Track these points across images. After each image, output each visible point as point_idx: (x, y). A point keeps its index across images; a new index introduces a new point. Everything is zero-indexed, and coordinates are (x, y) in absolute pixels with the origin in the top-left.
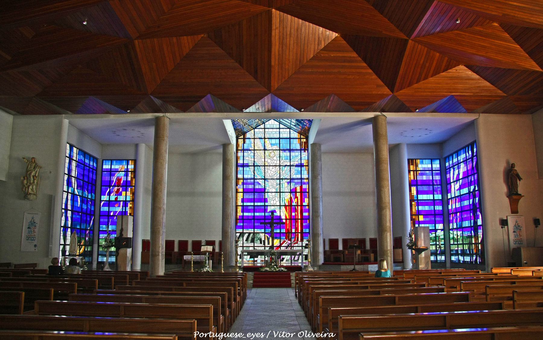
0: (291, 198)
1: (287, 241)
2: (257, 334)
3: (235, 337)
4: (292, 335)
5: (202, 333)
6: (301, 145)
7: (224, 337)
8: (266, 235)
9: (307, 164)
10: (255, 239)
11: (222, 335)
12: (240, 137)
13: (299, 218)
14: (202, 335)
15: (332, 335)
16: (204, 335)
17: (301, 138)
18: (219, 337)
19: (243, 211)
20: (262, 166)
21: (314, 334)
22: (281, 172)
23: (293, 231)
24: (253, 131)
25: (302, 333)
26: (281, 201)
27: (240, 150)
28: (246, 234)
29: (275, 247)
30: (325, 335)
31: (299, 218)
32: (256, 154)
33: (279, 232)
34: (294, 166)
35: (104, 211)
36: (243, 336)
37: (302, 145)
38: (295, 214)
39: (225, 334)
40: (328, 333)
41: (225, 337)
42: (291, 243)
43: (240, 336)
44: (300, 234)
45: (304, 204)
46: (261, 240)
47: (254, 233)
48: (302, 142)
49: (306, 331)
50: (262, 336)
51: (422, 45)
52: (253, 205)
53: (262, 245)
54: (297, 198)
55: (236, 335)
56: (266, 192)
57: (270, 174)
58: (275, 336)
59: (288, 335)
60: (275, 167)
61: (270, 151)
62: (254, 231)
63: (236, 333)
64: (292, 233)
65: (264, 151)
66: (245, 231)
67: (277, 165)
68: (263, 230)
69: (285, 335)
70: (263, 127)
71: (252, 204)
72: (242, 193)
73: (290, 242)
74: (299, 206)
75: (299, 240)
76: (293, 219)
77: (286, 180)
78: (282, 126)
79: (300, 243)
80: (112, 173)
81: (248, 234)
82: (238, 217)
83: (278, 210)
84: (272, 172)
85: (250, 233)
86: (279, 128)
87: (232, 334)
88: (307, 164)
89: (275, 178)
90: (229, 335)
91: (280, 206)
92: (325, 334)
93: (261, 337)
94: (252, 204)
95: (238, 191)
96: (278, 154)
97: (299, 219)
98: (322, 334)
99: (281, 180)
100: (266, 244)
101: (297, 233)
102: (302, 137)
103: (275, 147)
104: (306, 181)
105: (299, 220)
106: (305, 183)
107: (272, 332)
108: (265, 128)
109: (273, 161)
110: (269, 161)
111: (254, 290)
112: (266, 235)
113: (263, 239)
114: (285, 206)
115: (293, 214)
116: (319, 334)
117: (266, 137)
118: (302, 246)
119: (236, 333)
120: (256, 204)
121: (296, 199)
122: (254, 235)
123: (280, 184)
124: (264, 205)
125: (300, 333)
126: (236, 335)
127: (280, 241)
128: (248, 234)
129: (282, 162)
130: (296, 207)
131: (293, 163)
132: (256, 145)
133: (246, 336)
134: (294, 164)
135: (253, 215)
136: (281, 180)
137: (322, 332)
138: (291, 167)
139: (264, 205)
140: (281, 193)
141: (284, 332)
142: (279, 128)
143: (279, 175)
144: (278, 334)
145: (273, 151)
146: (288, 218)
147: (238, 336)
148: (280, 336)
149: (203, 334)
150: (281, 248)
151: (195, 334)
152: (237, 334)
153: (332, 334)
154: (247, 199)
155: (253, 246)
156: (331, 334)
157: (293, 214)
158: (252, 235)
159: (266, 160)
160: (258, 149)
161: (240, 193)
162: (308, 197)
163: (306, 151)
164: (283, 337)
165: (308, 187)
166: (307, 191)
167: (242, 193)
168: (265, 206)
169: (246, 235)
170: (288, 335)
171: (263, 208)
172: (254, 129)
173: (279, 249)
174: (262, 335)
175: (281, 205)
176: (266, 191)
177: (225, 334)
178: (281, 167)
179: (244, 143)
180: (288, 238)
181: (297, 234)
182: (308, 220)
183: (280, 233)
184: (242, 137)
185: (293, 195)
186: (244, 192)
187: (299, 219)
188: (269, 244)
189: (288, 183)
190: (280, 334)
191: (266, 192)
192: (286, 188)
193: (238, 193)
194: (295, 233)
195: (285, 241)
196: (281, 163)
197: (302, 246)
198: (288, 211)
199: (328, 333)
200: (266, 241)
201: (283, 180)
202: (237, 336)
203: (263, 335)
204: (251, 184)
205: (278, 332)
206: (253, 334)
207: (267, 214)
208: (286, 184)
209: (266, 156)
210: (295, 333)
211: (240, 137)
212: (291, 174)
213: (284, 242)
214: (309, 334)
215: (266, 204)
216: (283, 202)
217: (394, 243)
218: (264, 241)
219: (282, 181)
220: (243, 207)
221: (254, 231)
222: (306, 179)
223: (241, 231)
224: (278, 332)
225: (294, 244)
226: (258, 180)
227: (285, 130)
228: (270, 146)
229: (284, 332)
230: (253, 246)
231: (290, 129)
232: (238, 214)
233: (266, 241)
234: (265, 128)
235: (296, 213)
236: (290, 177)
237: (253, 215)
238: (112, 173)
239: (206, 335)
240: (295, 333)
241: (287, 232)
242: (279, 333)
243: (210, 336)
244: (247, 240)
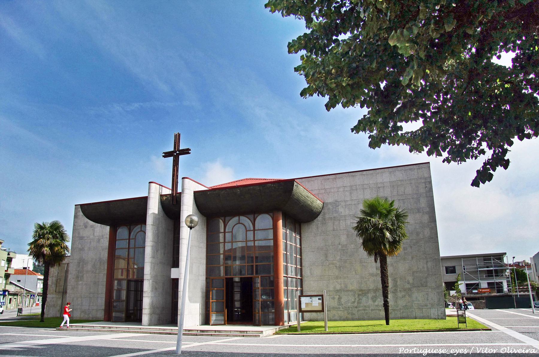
2: (461, 350)
3: (465, 353)
35: (143, 315)
40: (530, 349)
51: (114, 270)
55: (440, 351)
62: (254, 243)
80: (140, 283)
90: (433, 351)
92: (527, 350)
111: (504, 262)
125: (503, 349)
141: (487, 348)
152: (441, 350)
174: (440, 351)
206: (456, 350)
217: (277, 263)
221: (254, 243)
229: (487, 348)
238: (140, 283)
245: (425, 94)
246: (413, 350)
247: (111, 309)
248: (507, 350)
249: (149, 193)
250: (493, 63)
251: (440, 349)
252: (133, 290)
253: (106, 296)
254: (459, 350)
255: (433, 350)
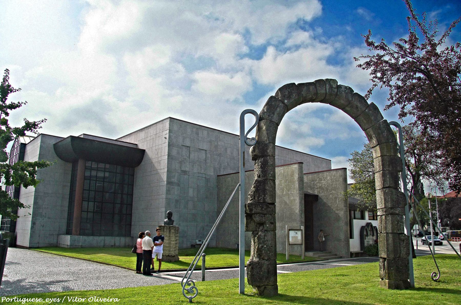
245: (393, 201)
246: (14, 299)
247: (329, 261)
248: (94, 300)
249: (419, 289)
250: (355, 180)
251: (37, 298)
252: (106, 166)
253: (6, 258)
254: (103, 299)
255: (20, 299)
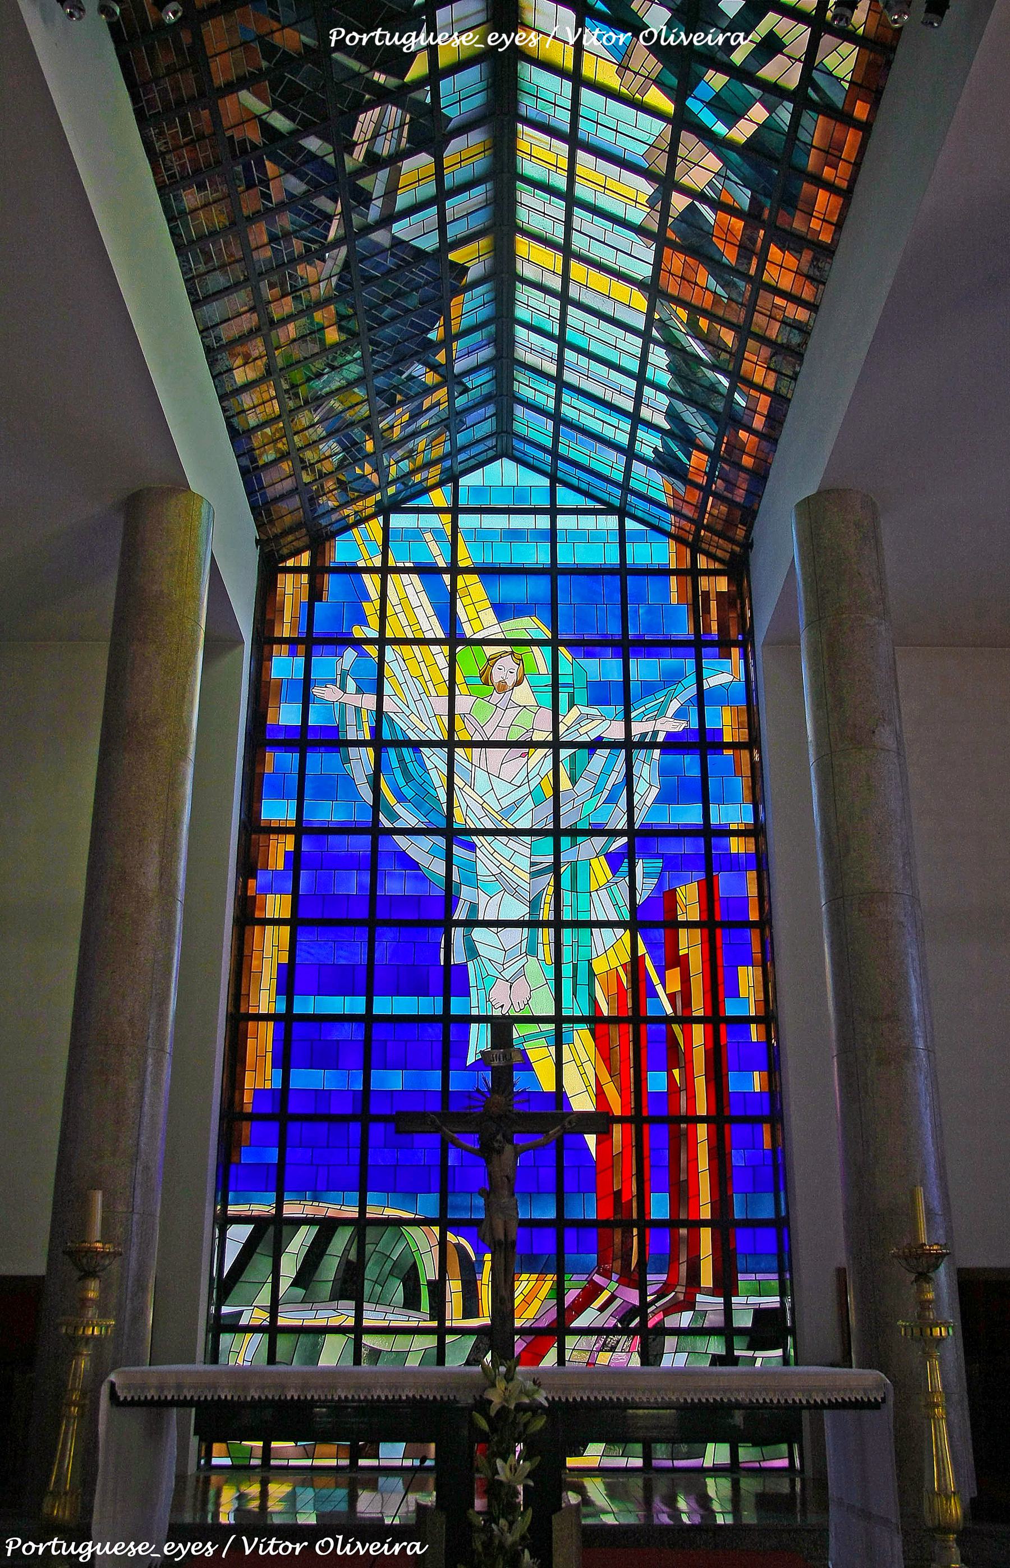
0: (635, 964)
1: (613, 1285)
4: (298, 1548)
5: (31, 1543)
6: (697, 604)
7: (93, 1554)
8: (451, 1237)
9: (743, 736)
10: (371, 1272)
11: (89, 1548)
12: (290, 563)
13: (702, 1109)
14: (29, 1549)
15: (417, 1548)
16: (37, 1549)
17: (694, 573)
18: (79, 1554)
19: (284, 1060)
20: (430, 744)
21: (363, 1548)
22: (565, 783)
23: (659, 1206)
24: (375, 526)
25: (327, 1543)
26: (567, 985)
27: (282, 641)
28: (304, 1229)
29: (523, 1331)
30: (397, 1548)
31: (702, 1110)
32: (394, 665)
33: (551, 1214)
34: (653, 745)
36: (151, 1552)
37: (707, 610)
38: (671, 1078)
39: (100, 1544)
40: (405, 1544)
41: (99, 1553)
42: (644, 1305)
43: (143, 1551)
44: (706, 1235)
45: (731, 1008)
46: (411, 1278)
47: (361, 1224)
48: (706, 594)
49: (340, 1537)
50: (210, 1550)
52: (361, 1010)
53: (421, 1318)
54: (682, 962)
55: (130, 1550)
56: (459, 923)
57: (490, 798)
58: (248, 1552)
59: (286, 1549)
60: (523, 755)
61: (490, 650)
63: (133, 1543)
64: (645, 1223)
65: (446, 649)
66: (291, 1210)
67: (538, 737)
68: (428, 1204)
69: (276, 1547)
70: (443, 504)
71: (354, 1005)
72: (286, 930)
73: (633, 1297)
74: (698, 1020)
75: (707, 1279)
76: (653, 1120)
77: (599, 841)
78: (566, 498)
79: (710, 1303)
81: (315, 1229)
82: (248, 1098)
83: (544, 1052)
84: (501, 788)
85: (328, 1227)
86: (553, 511)
87: (121, 1545)
88: (743, 736)
89: (525, 824)
91: (558, 1019)
92: (397, 1544)
93: (206, 1554)
94: (354, 1005)
95: (258, 915)
96: (543, 670)
97: (702, 1119)
98: (386, 1546)
99: (565, 841)
100: (454, 1316)
101: (684, 1224)
102: (703, 562)
103: (526, 622)
104: (736, 846)
105: (702, 1130)
106: (733, 863)
107: (238, 1543)
108: (455, 510)
109: (511, 713)
110: (483, 712)
112: (451, 1237)
113: (429, 1271)
114: (595, 1021)
115: (657, 1082)
116: (379, 1545)
117: (462, 564)
118: (727, 1331)
119: (133, 1543)
120: (385, 1005)
121: (674, 975)
122: (360, 1239)
123: (557, 865)
124: (439, 1011)
125: (323, 1541)
126: (132, 1548)
127: (559, 1290)
128: (315, 1229)
129: (568, 718)
130: (676, 1028)
131: (647, 727)
132: (398, 609)
133: (161, 1552)
134: (655, 733)
135: (359, 1087)
136: (565, 841)
137: (388, 1541)
138: (635, 752)
139: (439, 1011)
140: (567, 934)
142: (553, 511)
143: (550, 803)
144: (257, 1546)
145: (508, 649)
146: (617, 1111)
147: (137, 1551)
148: (261, 1553)
149: (34, 1546)
150: (570, 1341)
151: (8, 1545)
152: (135, 1546)
153: (418, 1544)
154: (321, 967)
155: (351, 1322)
156: (413, 1546)
157: (657, 1082)
158: (341, 1240)
159: (462, 704)
160: (410, 636)
161: (269, 929)
162: (757, 956)
163: (735, 652)
164: (272, 1553)
165: (752, 890)
166: (754, 916)
167: (286, 930)
168: (446, 1017)
169: (301, 1240)
170: (286, 1549)
171: (435, 1032)
172: (385, 510)
173: (550, 1360)
175: (565, 1013)
176: (460, 914)
177: (100, 1544)
178: (564, 753)
179: (315, 594)
180: (618, 1264)
181: (683, 1231)
182: (766, 1128)
183: (560, 1223)
184: (305, 559)
185: (649, 946)
186: (296, 922)
187: (702, 1119)
188: (470, 1309)
189: (614, 861)
190: (261, 1546)
191: (459, 923)
192: (603, 893)
193: (257, 929)
194: (672, 1224)
195: (599, 1289)
196: (562, 728)
197: (727, 1331)
198: (616, 1057)
199: (405, 1544)
200: (454, 1287)
201: (580, 839)
202: (134, 1551)
203: (212, 1547)
204: (350, 862)
205: (256, 1539)
207: (458, 1081)
208: (601, 869)
209: (459, 678)
210: (306, 1544)
211: (290, 563)
212: (636, 798)
213: (591, 1292)
214: (349, 1546)
215: (457, 1006)
216: (583, 992)
218: (438, 1289)
219: (574, 844)
220: (288, 1032)
222: (737, 833)
223: (262, 1207)
224: (256, 1539)
225: (668, 1311)
226: (402, 842)
227: (587, 522)
228: (489, 616)
229: (274, 1539)
230: (351, 1322)
231: (622, 513)
232: (251, 1081)
233: (454, 1287)
234: (455, 510)
235: (676, 1072)
236: (631, 820)
237: (359, 1087)
239: (41, 1548)
240: (306, 1544)
241: (609, 1215)
242: (259, 1542)
243: (54, 1553)
244: (304, 1277)
